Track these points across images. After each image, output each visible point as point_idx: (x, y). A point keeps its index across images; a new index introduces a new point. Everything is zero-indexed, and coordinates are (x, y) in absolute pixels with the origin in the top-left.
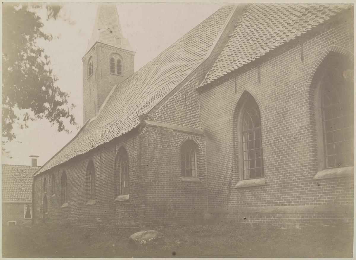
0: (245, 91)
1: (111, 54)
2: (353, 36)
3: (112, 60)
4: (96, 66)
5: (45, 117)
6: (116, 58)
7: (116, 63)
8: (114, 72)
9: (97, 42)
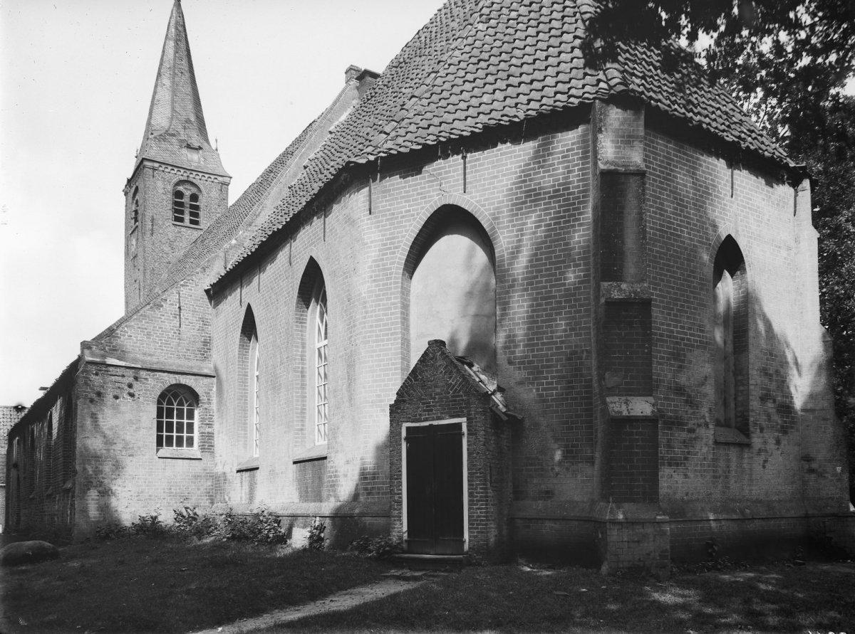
3: (179, 194)
6: (187, 191)
8: (182, 220)
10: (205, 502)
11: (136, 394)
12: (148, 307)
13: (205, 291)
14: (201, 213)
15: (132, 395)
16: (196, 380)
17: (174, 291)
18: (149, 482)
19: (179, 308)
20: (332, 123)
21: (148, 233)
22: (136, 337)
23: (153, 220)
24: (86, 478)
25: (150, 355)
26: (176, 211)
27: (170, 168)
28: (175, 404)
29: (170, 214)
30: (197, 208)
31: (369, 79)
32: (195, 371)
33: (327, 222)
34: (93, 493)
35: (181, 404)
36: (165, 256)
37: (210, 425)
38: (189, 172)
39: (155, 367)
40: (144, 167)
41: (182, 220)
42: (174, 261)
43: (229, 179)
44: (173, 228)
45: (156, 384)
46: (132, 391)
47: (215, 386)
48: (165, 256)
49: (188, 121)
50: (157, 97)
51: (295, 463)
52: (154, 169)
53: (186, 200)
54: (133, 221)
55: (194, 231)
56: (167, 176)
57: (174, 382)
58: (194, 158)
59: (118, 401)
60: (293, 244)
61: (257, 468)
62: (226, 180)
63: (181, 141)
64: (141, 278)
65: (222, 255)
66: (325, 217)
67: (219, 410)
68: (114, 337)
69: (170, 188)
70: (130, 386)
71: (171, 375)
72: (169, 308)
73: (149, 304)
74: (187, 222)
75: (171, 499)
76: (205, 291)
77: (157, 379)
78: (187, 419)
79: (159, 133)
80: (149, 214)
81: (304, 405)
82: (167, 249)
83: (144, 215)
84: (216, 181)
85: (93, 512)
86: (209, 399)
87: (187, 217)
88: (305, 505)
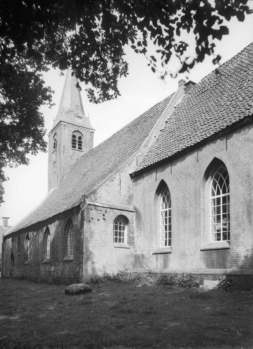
0: (215, 157)
1: (74, 132)
2: (141, 116)
3: (74, 136)
4: (60, 142)
5: (109, 70)
6: (77, 135)
7: (77, 139)
8: (75, 147)
9: (61, 121)
10: (131, 267)
11: (106, 219)
12: (109, 181)
13: (130, 174)
14: (83, 144)
15: (104, 219)
16: (128, 213)
17: (118, 174)
18: (111, 258)
19: (120, 181)
20: (175, 103)
21: (62, 152)
22: (104, 194)
23: (64, 147)
24: (87, 256)
25: (109, 202)
26: (73, 143)
27: (71, 125)
28: (118, 224)
29: (71, 145)
30: (81, 142)
31: (191, 85)
32: (127, 209)
33: (228, 144)
34: (89, 263)
35: (120, 224)
36: (68, 162)
37: (133, 233)
38: (78, 127)
39: (113, 207)
40: (61, 124)
41: (75, 147)
42: (72, 164)
43: (94, 130)
44: (72, 150)
45: (112, 215)
46: (104, 218)
47: (135, 216)
48: (68, 162)
49: (77, 106)
50: (64, 96)
51: (201, 250)
52: (65, 125)
53: (77, 139)
54: (53, 148)
55: (80, 152)
56: (70, 129)
57: (120, 214)
58: (79, 122)
59: (99, 221)
60: (199, 153)
61: (171, 253)
62: (93, 131)
63: (75, 114)
64: (59, 171)
65: (136, 159)
66: (227, 139)
67: (138, 227)
68: (96, 193)
69: (71, 134)
70: (104, 215)
71: (119, 211)
72: (116, 181)
73: (109, 179)
74: (77, 148)
75: (119, 266)
76: (130, 174)
77: (114, 212)
78: (117, 232)
79: (66, 111)
80: (62, 144)
81: (204, 225)
82: (69, 159)
83: (60, 145)
84: (89, 131)
85: (90, 272)
86: (132, 222)
87: (77, 146)
88: (208, 269)
